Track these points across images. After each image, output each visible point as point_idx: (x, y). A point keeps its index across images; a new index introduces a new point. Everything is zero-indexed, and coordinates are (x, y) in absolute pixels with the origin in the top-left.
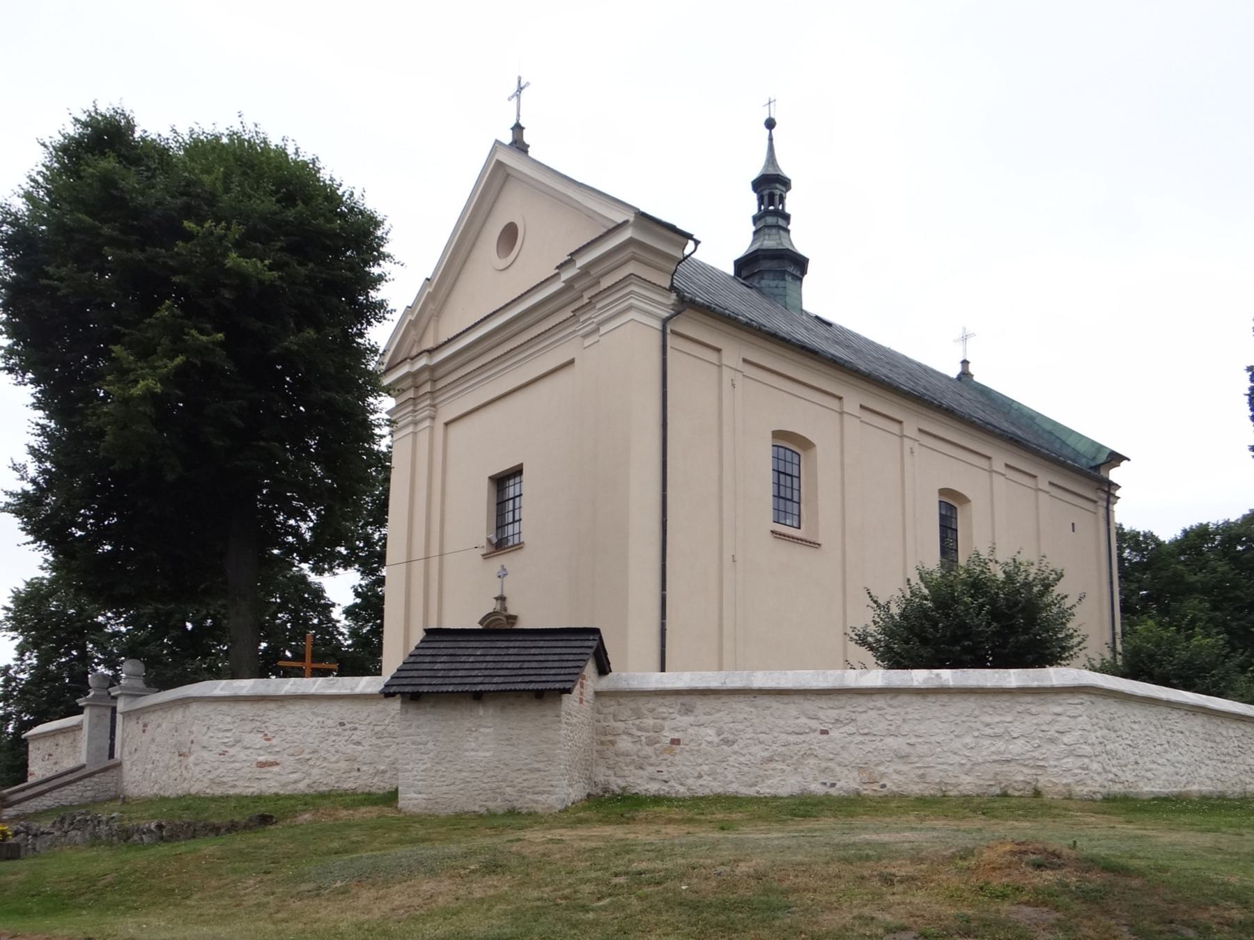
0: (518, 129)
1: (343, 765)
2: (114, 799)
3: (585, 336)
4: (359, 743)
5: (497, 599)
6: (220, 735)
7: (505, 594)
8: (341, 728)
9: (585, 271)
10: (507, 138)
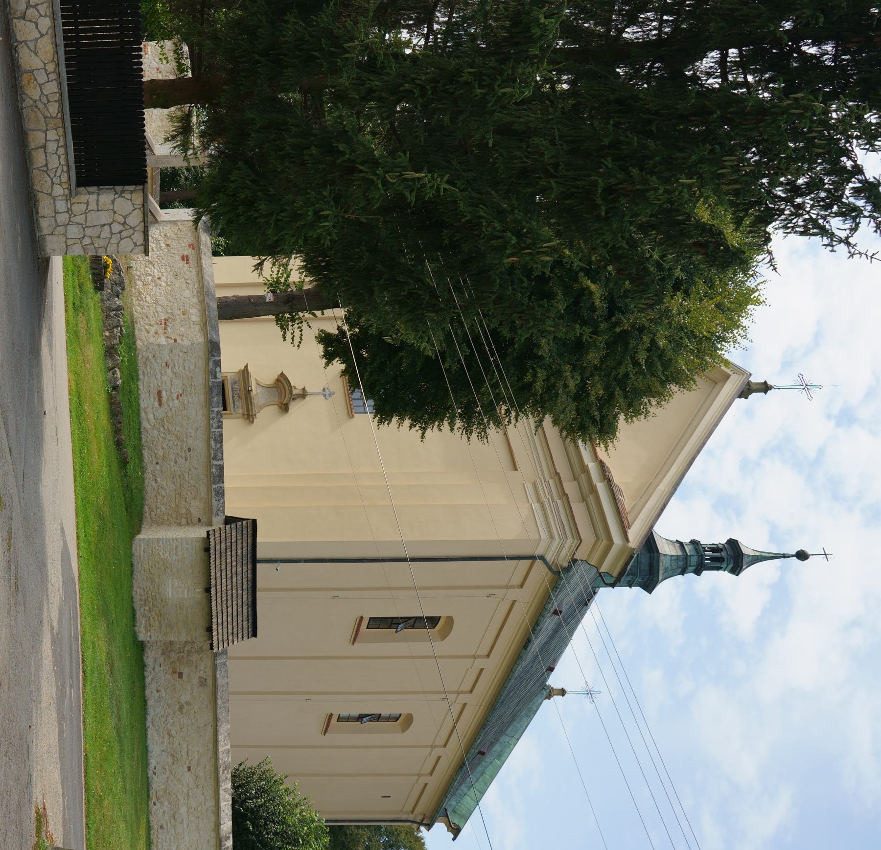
0: (765, 388)
1: (161, 453)
3: (535, 485)
4: (176, 462)
5: (304, 390)
6: (181, 362)
7: (308, 398)
8: (186, 449)
9: (593, 490)
10: (756, 379)
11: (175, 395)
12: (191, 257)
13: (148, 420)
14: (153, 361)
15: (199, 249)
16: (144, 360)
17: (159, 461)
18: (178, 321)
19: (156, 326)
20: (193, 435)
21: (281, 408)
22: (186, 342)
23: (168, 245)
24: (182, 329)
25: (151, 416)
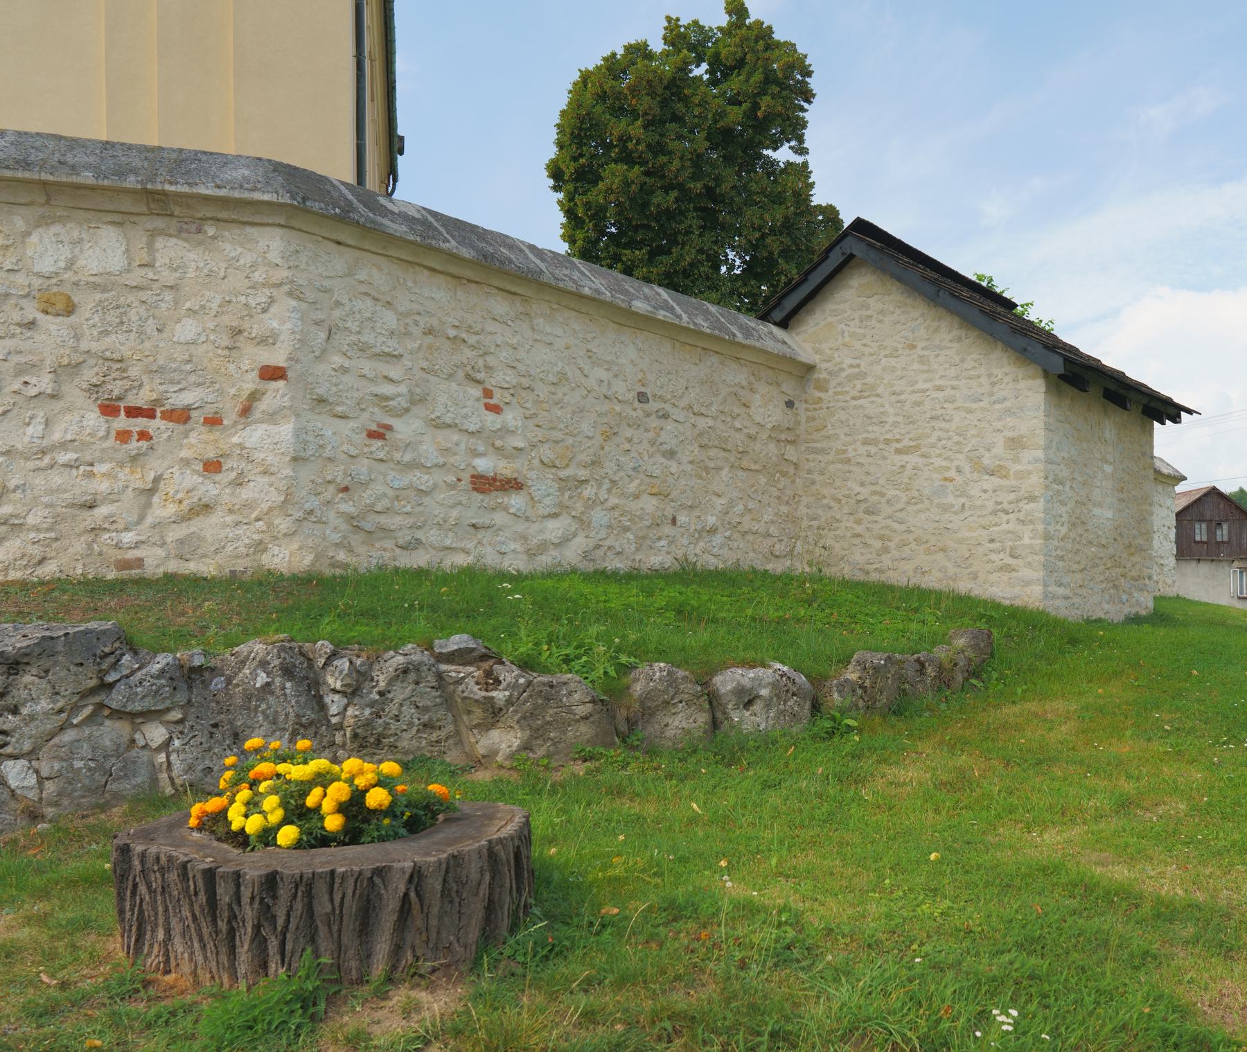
2: (309, 659)
4: (671, 454)
6: (368, 367)
11: (490, 416)
13: (565, 540)
14: (367, 496)
16: (356, 540)
17: (669, 512)
22: (282, 320)
25: (555, 529)
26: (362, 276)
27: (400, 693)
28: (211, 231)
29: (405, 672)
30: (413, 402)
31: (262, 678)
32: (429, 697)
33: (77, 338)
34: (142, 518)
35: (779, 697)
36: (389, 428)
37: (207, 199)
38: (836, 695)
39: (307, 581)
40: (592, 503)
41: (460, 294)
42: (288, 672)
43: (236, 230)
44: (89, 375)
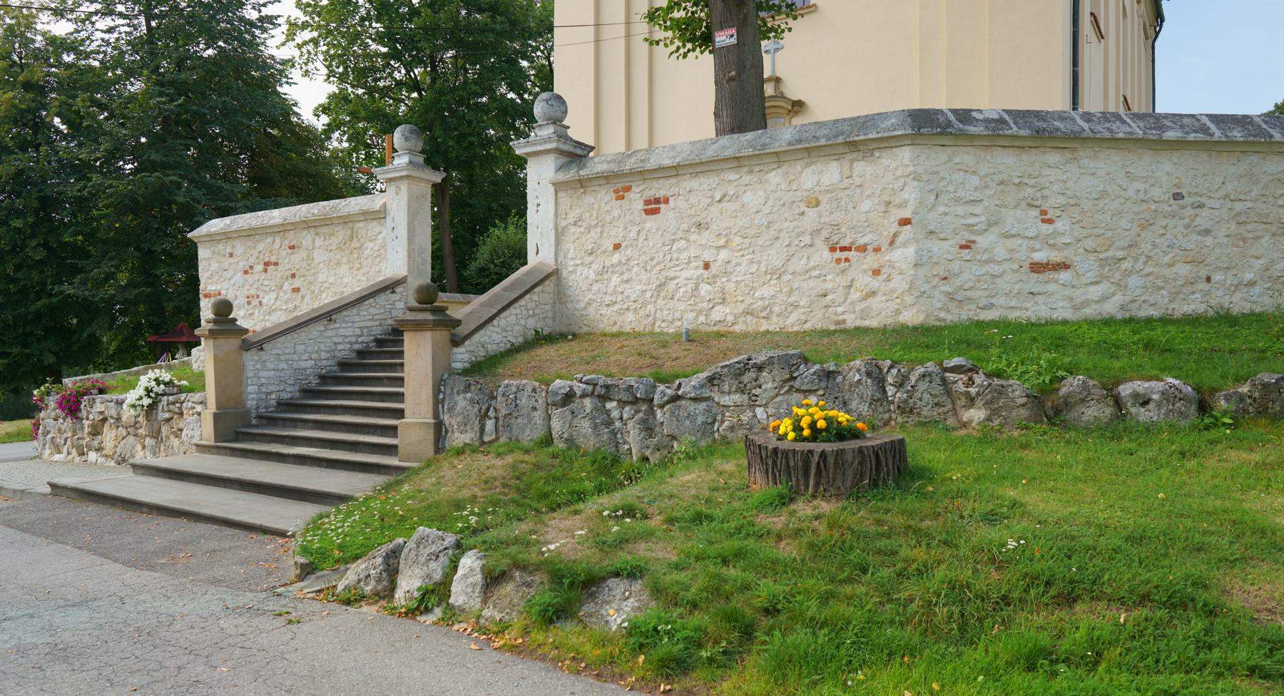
1: (1183, 270)
4: (1207, 232)
6: (960, 210)
11: (1046, 226)
12: (650, 194)
13: (1104, 299)
15: (631, 173)
16: (952, 305)
17: (1204, 273)
18: (838, 217)
19: (852, 274)
20: (1140, 186)
21: (797, 113)
22: (911, 194)
23: (617, 247)
24: (866, 206)
25: (1094, 292)
26: (957, 160)
27: (922, 387)
28: (877, 154)
29: (924, 376)
30: (990, 225)
31: (857, 377)
32: (938, 390)
33: (820, 217)
34: (846, 300)
35: (1168, 401)
36: (974, 242)
37: (873, 140)
38: (1222, 402)
39: (920, 330)
40: (1129, 273)
41: (1024, 157)
42: (869, 374)
43: (888, 151)
44: (825, 234)
